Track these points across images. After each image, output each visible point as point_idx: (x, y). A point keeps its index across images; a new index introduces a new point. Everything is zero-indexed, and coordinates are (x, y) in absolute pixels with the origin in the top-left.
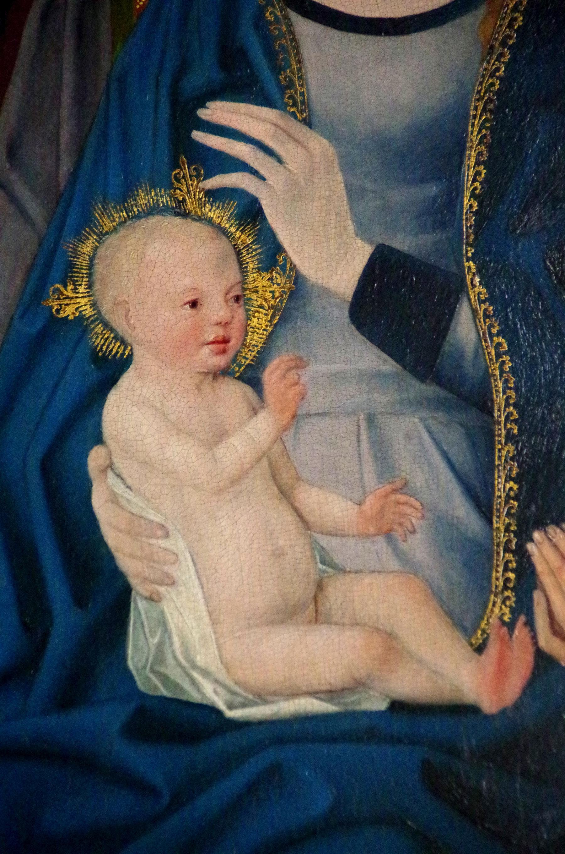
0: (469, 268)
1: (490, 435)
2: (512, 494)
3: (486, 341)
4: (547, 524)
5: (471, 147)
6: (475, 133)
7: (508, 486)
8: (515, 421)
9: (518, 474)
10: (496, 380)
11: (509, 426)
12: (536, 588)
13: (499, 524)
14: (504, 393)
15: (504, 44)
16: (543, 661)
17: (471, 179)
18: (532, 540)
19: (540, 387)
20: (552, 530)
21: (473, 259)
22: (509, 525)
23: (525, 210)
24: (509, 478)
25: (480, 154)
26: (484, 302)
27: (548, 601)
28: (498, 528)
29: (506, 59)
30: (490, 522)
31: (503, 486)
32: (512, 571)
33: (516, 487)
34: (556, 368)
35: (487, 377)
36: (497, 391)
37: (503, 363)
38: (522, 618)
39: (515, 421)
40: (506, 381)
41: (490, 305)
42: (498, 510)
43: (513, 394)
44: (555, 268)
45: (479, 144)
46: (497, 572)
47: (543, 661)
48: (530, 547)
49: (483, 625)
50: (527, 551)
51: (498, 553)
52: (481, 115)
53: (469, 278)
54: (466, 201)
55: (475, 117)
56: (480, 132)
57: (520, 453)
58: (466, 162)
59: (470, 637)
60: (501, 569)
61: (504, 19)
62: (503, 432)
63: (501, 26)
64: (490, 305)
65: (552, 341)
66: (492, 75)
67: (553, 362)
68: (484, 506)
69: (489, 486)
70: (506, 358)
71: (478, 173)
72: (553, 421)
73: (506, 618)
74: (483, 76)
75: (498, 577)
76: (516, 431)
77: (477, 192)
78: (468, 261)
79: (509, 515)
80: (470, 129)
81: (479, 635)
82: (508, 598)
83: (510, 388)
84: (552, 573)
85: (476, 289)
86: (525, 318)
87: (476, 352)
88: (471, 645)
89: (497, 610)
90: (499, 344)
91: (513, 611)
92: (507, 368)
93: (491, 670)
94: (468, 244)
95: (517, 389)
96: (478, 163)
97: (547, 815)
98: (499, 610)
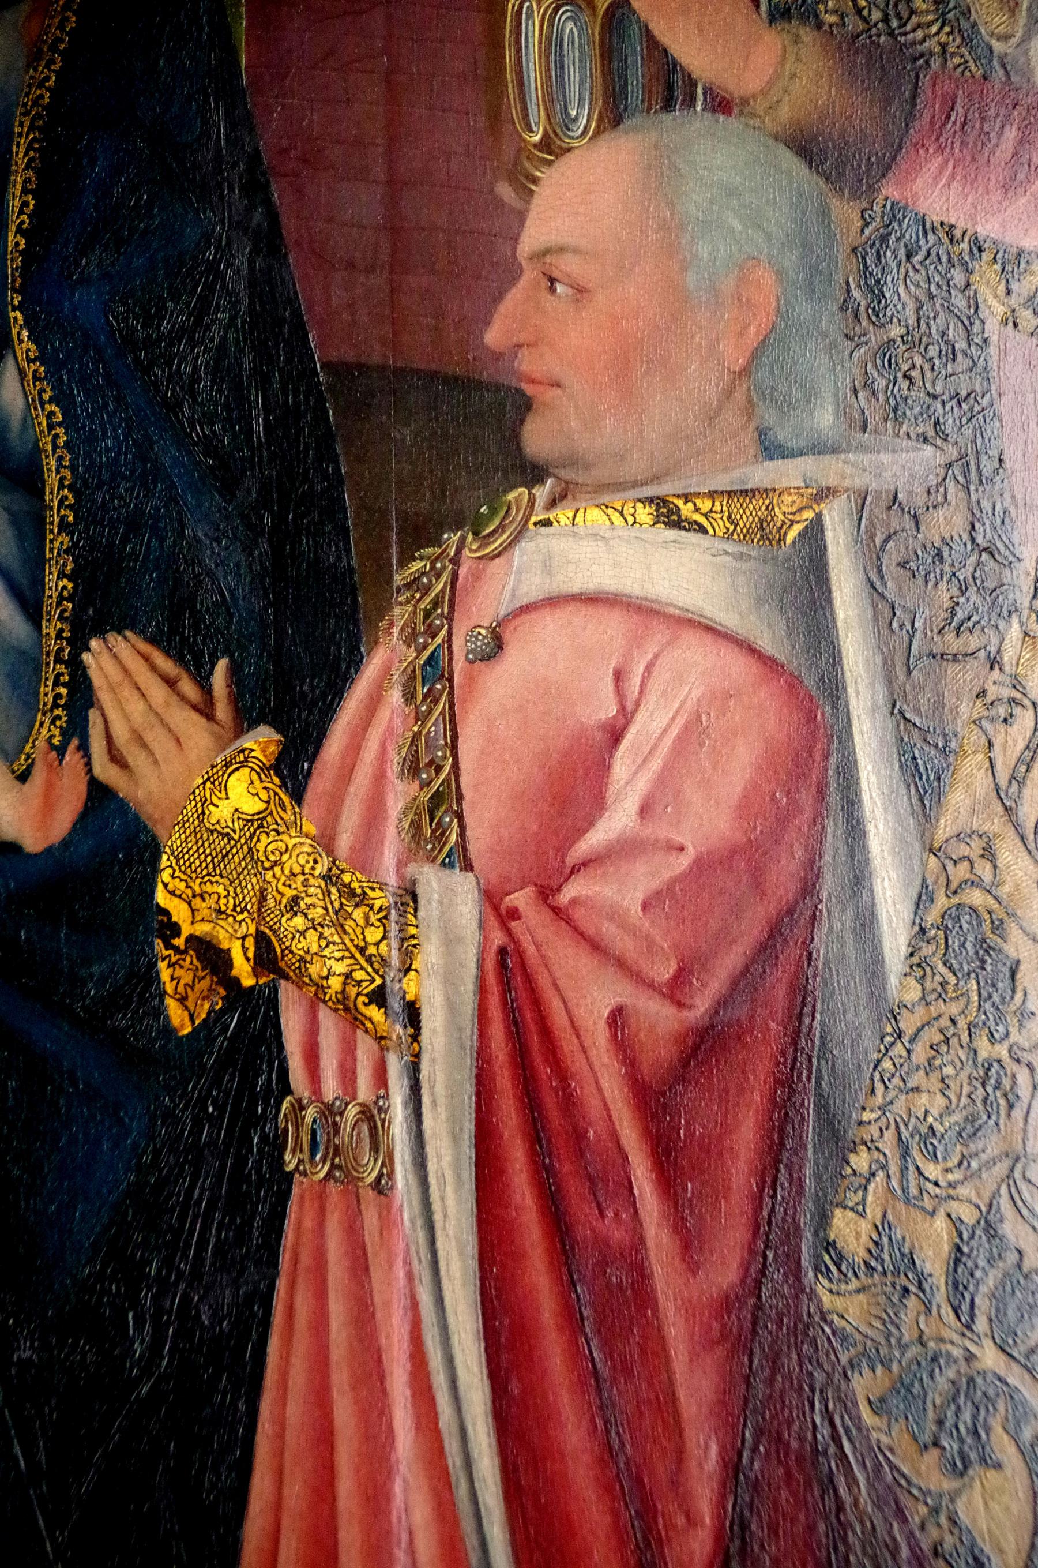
0: (15, 318)
1: (40, 523)
2: (65, 593)
3: (36, 409)
4: (107, 632)
5: (17, 171)
6: (21, 155)
7: (61, 584)
8: (70, 507)
9: (72, 570)
10: (47, 457)
11: (63, 512)
12: (92, 706)
13: (50, 628)
14: (58, 472)
15: (53, 48)
16: (99, 793)
17: (17, 210)
18: (88, 649)
19: (101, 467)
20: (112, 638)
21: (20, 308)
22: (61, 631)
23: (83, 253)
24: (61, 575)
25: (27, 181)
26: (33, 361)
27: (106, 722)
28: (48, 634)
29: (56, 67)
30: (39, 628)
31: (55, 584)
32: (64, 685)
33: (70, 586)
34: (120, 444)
35: (37, 451)
36: (49, 470)
37: (56, 436)
38: (75, 742)
39: (70, 507)
40: (60, 459)
41: (41, 365)
42: (49, 613)
43: (67, 473)
44: (119, 324)
45: (27, 168)
46: (46, 686)
47: (99, 793)
48: (86, 657)
49: (27, 749)
50: (82, 662)
51: (48, 664)
52: (28, 135)
53: (15, 331)
54: (11, 238)
55: (20, 135)
56: (26, 154)
57: (75, 545)
58: (11, 190)
59: (12, 763)
60: (50, 683)
61: (52, 18)
62: (56, 520)
63: (49, 26)
64: (41, 365)
65: (115, 412)
66: (41, 85)
67: (116, 437)
68: (31, 608)
69: (39, 583)
70: (60, 431)
71: (25, 204)
72: (115, 509)
73: (55, 741)
74: (30, 86)
75: (47, 692)
76: (71, 519)
77: (25, 226)
78: (14, 310)
79: (61, 618)
80: (14, 149)
81: (22, 761)
82: (59, 717)
83: (65, 467)
84: (112, 689)
85: (24, 345)
86: (83, 381)
87: (24, 420)
88: (13, 772)
89: (44, 731)
90: (52, 414)
91: (63, 732)
92: (61, 442)
93: (36, 802)
94: (14, 290)
95: (73, 468)
96: (25, 191)
97: (96, 969)
98: (47, 731)
